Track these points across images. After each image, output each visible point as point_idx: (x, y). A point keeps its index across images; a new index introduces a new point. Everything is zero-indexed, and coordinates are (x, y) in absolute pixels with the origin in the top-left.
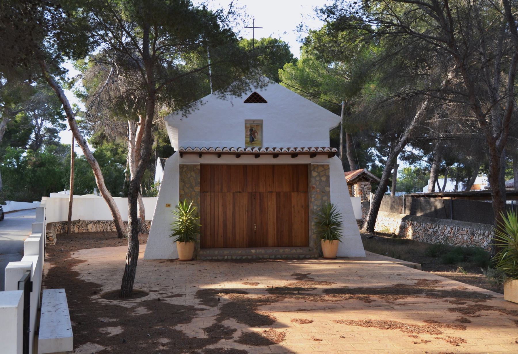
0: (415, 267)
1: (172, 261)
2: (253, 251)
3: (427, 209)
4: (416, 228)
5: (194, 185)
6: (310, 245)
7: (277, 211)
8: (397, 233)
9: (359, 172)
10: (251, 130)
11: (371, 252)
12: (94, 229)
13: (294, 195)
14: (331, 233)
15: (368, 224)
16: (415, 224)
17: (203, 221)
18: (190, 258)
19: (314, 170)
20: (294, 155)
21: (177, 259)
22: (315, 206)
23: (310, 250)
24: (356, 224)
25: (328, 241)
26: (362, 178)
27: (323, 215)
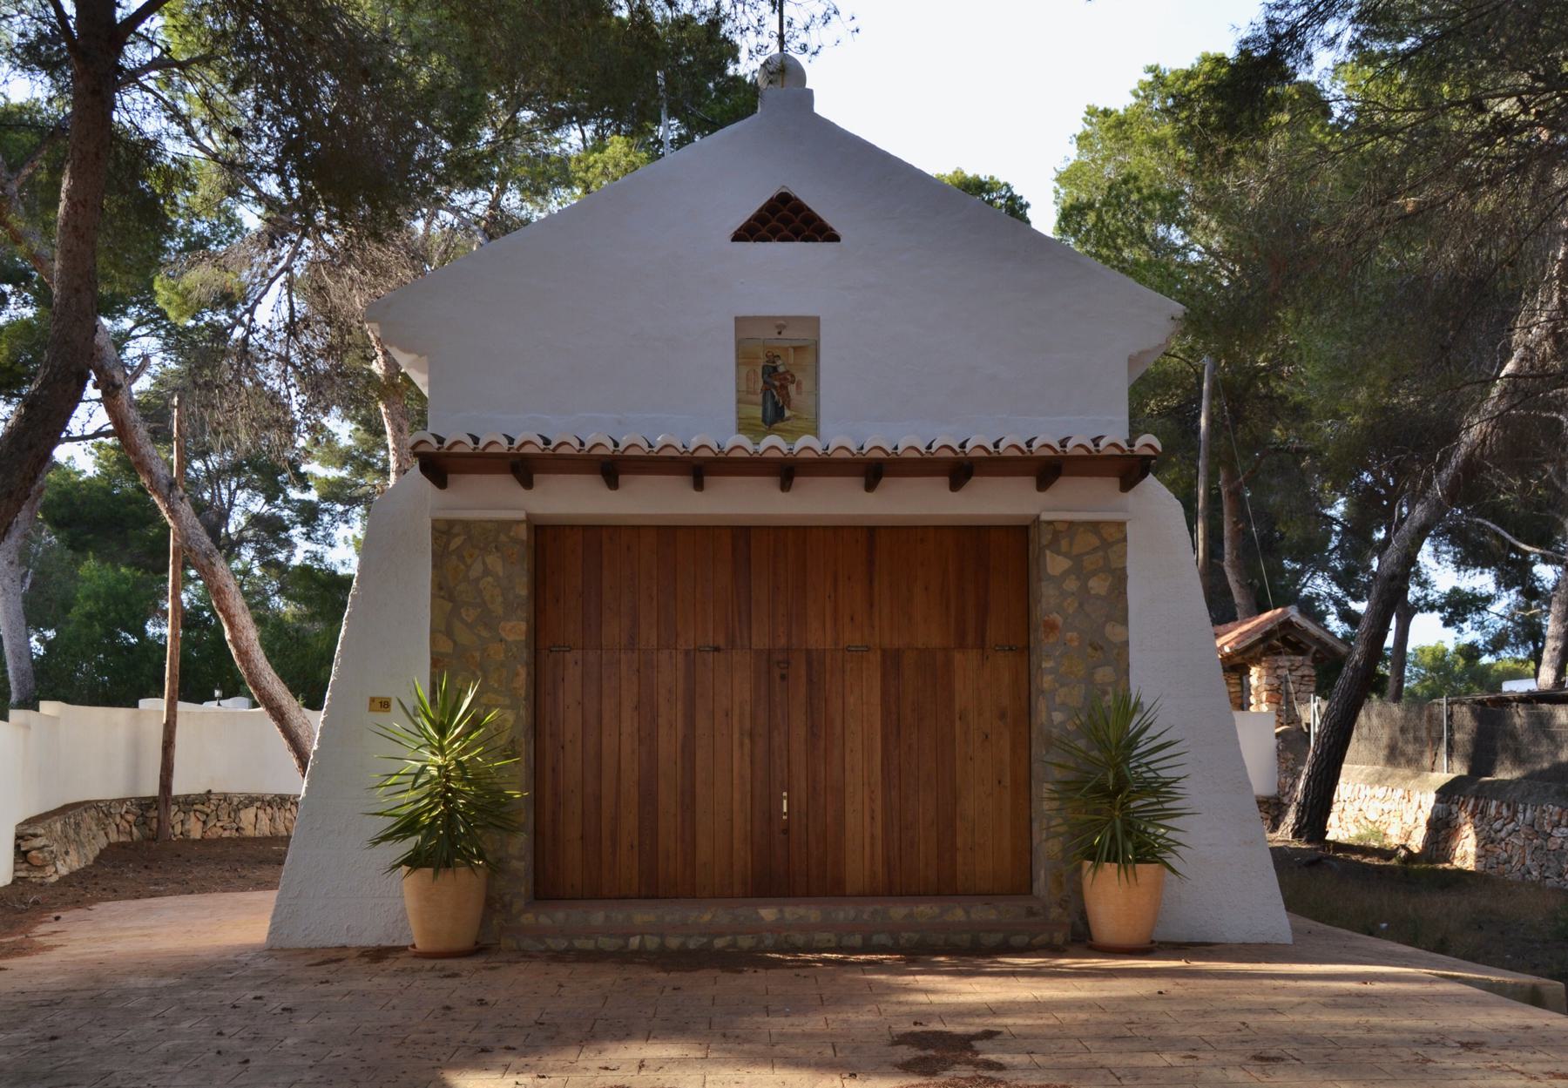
0: (1535, 998)
1: (378, 954)
2: (768, 914)
3: (1540, 756)
4: (1497, 825)
5: (500, 611)
6: (1035, 886)
7: (885, 738)
8: (1416, 844)
9: (1270, 620)
10: (770, 371)
11: (1316, 919)
12: (265, 828)
13: (965, 663)
14: (1127, 834)
15: (1302, 808)
16: (1493, 811)
17: (540, 774)
18: (465, 940)
19: (1054, 544)
20: (959, 470)
21: (405, 949)
22: (1056, 711)
23: (1031, 912)
24: (1256, 814)
25: (1110, 869)
26: (1279, 643)
27: (1095, 753)
